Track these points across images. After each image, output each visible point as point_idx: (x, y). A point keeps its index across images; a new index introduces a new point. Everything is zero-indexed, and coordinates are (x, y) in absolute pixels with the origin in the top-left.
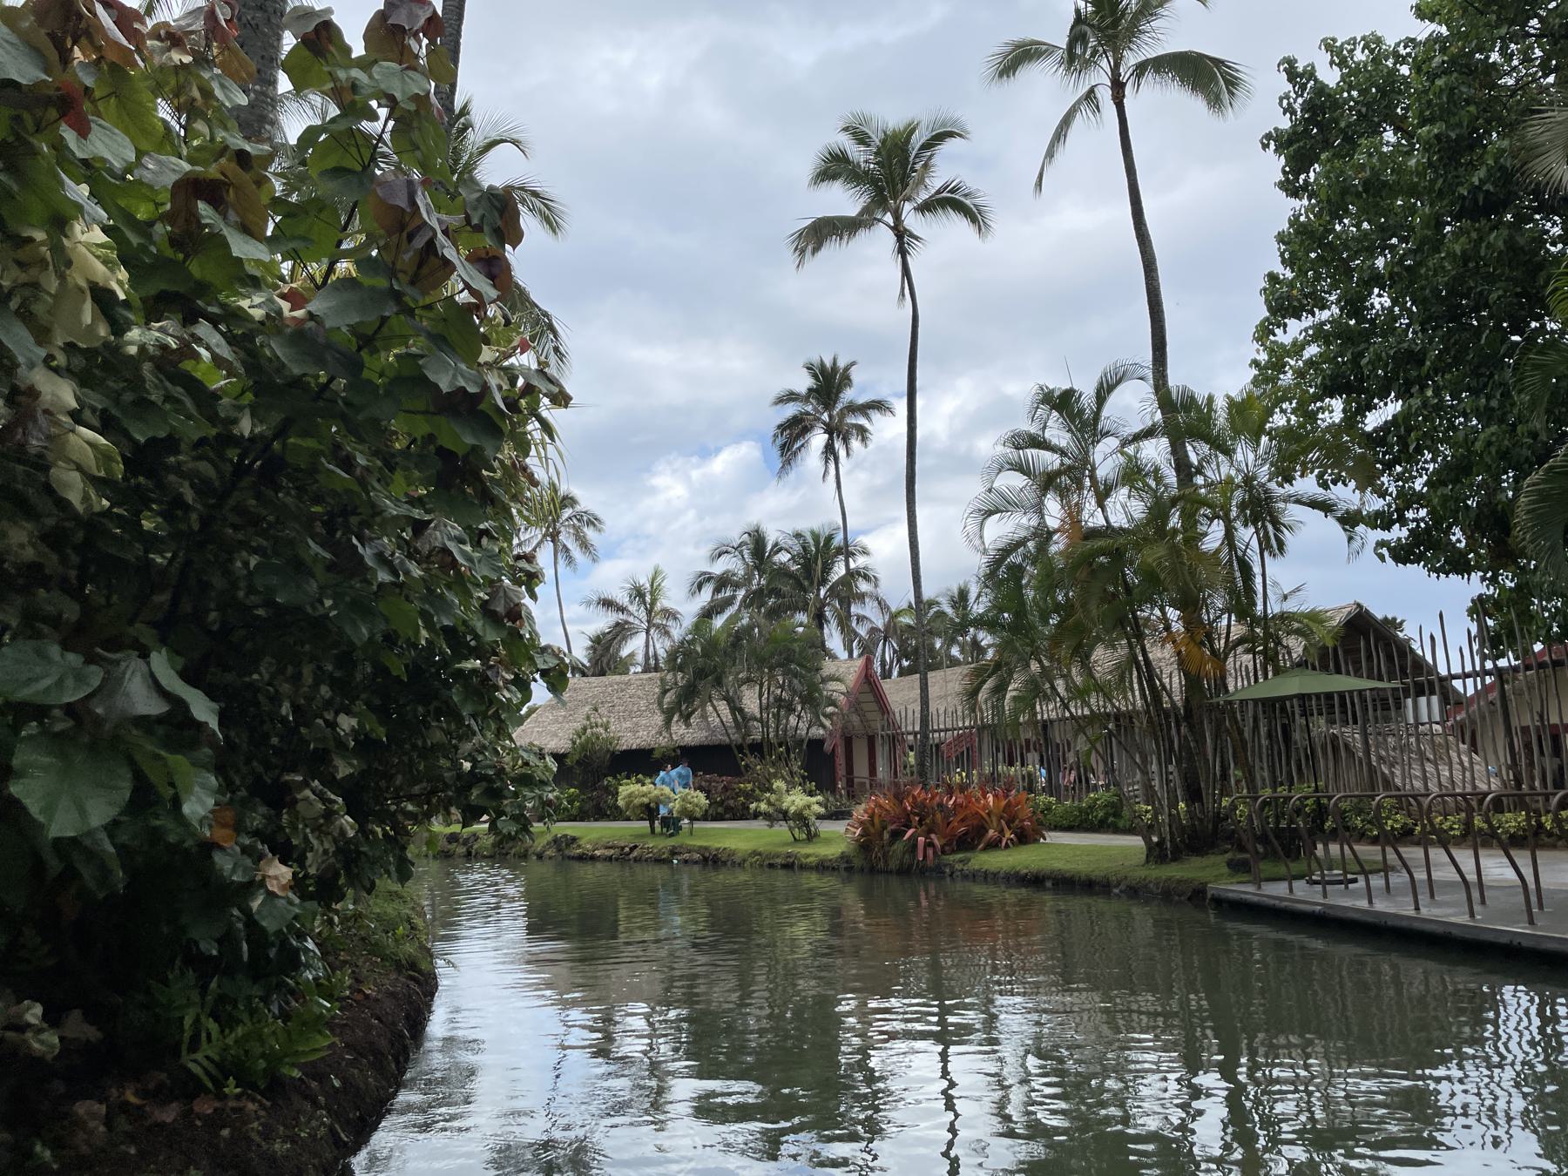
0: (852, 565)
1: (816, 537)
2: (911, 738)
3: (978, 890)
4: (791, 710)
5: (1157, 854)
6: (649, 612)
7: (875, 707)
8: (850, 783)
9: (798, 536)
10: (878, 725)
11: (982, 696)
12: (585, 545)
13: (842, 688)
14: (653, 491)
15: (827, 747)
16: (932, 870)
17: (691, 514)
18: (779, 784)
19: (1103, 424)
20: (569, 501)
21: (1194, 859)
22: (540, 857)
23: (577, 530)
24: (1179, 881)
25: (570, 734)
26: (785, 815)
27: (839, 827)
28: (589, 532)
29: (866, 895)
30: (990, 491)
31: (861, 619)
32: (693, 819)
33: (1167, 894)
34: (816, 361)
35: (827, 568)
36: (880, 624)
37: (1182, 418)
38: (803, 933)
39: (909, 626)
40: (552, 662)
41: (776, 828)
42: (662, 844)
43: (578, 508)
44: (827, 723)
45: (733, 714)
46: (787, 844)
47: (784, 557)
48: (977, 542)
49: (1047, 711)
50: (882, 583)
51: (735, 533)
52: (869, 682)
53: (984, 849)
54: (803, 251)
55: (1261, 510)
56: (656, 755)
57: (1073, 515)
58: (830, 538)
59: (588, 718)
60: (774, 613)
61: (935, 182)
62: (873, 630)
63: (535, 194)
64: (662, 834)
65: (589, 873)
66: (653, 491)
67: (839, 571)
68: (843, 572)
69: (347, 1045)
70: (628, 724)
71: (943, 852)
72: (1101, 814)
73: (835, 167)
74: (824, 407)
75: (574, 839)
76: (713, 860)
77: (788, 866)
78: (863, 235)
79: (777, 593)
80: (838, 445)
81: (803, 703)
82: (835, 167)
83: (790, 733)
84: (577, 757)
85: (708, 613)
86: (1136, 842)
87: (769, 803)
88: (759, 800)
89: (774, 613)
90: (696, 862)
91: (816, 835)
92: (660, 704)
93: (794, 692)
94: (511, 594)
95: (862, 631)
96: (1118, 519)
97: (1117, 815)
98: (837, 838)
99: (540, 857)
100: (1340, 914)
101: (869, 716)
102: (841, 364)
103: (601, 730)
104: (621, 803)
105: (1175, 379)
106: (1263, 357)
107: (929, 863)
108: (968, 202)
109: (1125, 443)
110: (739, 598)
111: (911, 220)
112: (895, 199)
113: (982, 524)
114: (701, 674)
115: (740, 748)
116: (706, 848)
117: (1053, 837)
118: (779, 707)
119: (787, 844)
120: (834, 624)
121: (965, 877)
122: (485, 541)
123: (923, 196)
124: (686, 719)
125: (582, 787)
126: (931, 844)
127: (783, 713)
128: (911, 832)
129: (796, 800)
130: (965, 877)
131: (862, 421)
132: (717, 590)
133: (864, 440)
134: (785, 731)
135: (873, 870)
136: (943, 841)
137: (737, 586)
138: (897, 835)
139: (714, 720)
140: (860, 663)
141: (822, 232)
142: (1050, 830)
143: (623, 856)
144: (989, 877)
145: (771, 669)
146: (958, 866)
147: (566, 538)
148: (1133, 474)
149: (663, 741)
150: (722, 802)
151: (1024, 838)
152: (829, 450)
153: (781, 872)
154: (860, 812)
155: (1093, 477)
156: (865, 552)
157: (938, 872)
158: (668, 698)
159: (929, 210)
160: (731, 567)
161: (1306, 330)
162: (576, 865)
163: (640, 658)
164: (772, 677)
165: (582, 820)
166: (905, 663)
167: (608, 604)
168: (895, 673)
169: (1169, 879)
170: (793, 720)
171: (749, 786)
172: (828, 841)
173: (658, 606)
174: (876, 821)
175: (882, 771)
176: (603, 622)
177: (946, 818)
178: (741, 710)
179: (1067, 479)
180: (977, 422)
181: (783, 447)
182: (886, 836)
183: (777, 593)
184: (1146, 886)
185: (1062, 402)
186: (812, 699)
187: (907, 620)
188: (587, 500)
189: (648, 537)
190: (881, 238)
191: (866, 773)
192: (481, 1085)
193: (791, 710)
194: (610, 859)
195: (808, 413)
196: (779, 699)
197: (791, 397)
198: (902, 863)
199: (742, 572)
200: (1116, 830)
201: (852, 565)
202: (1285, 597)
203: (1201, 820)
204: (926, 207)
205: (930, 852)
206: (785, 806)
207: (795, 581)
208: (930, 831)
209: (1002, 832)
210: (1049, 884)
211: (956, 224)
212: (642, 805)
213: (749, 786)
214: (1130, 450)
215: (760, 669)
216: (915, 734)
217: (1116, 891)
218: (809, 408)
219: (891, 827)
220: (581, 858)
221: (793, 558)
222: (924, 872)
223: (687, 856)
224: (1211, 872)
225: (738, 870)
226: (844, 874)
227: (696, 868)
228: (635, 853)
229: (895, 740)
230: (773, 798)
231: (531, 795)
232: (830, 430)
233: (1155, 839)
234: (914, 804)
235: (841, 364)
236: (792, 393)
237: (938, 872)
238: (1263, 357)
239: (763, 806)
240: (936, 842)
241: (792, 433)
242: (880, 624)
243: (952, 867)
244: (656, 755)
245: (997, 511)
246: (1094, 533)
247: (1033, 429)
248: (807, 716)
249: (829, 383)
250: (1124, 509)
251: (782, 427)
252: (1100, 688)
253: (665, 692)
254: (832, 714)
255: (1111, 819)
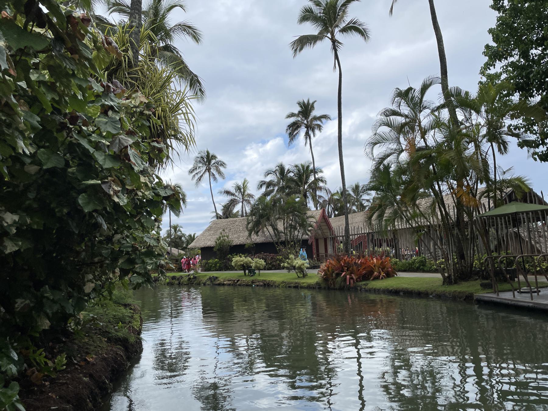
0: (317, 176)
1: (303, 166)
2: (341, 238)
3: (372, 297)
4: (295, 228)
5: (447, 281)
6: (243, 195)
7: (326, 227)
8: (318, 255)
9: (296, 166)
10: (328, 234)
11: (374, 217)
12: (220, 172)
13: (315, 220)
14: (246, 156)
15: (309, 242)
16: (352, 288)
17: (259, 164)
18: (291, 256)
19: (425, 103)
20: (214, 157)
21: (463, 283)
22: (205, 284)
23: (217, 167)
24: (459, 292)
25: (215, 239)
26: (294, 268)
27: (315, 272)
28: (221, 169)
29: (328, 300)
30: (375, 134)
31: (320, 197)
32: (259, 269)
33: (455, 298)
34: (301, 101)
35: (308, 177)
36: (327, 199)
37: (454, 99)
38: (304, 311)
39: (338, 199)
40: (169, 193)
41: (291, 272)
42: (249, 279)
43: (217, 160)
44: (309, 233)
45: (274, 231)
46: (296, 279)
47: (291, 174)
48: (371, 156)
49: (399, 225)
50: (328, 183)
51: (273, 166)
52: (325, 218)
53: (373, 280)
54: (296, 50)
55: (494, 135)
56: (246, 247)
57: (412, 143)
58: (308, 167)
59: (221, 234)
60: (288, 194)
61: (347, 19)
62: (325, 201)
63: (190, 27)
64: (249, 275)
65: (222, 290)
66: (246, 156)
67: (312, 179)
68: (313, 179)
69: (60, 397)
70: (236, 236)
71: (357, 281)
72: (417, 265)
73: (307, 16)
74: (305, 119)
75: (217, 278)
76: (267, 285)
77: (296, 287)
78: (319, 43)
79: (290, 188)
80: (311, 132)
81: (300, 226)
82: (307, 16)
83: (295, 238)
84: (217, 248)
85: (266, 194)
86: (439, 276)
87: (288, 263)
88: (284, 262)
89: (288, 194)
90: (261, 286)
91: (306, 275)
92: (247, 228)
93: (296, 222)
94: (123, 142)
95: (321, 201)
96: (431, 142)
97: (424, 265)
98: (315, 276)
99: (205, 284)
100: (542, 307)
101: (325, 231)
102: (311, 102)
103: (226, 238)
104: (233, 264)
105: (452, 84)
106: (484, 79)
107: (352, 285)
108: (360, 28)
109: (433, 111)
110: (276, 190)
111: (338, 36)
112: (331, 27)
113: (373, 148)
114: (261, 216)
115: (277, 243)
116: (265, 281)
117: (401, 275)
118: (291, 228)
119: (296, 279)
120: (310, 198)
121: (366, 291)
122: (110, 113)
123: (342, 25)
124: (257, 233)
125: (220, 259)
126: (352, 278)
127: (292, 230)
128: (344, 274)
129: (298, 262)
130: (366, 291)
131: (319, 122)
132: (268, 187)
133: (320, 130)
134: (293, 237)
135: (329, 289)
136: (357, 277)
137: (274, 185)
138: (338, 275)
139: (267, 233)
140: (321, 211)
141: (303, 42)
142: (397, 272)
143: (234, 284)
144: (377, 291)
145: (287, 214)
146: (364, 287)
147: (213, 170)
148: (437, 124)
149: (249, 241)
150: (271, 263)
151: (389, 275)
152: (307, 135)
153: (293, 290)
154: (323, 266)
155: (420, 125)
156: (321, 172)
157: (355, 289)
158: (250, 225)
159: (345, 31)
160: (272, 179)
161: (503, 67)
162: (217, 287)
163: (240, 213)
164: (288, 217)
165: (220, 270)
166: (337, 213)
167: (228, 193)
168: (333, 216)
169: (455, 291)
170: (296, 233)
171: (281, 257)
172: (311, 277)
173: (246, 193)
174: (330, 269)
175: (330, 251)
176: (226, 199)
177: (358, 267)
178: (277, 230)
179: (410, 126)
180: (360, 128)
181: (290, 134)
182: (334, 275)
183: (290, 188)
184: (444, 294)
185: (404, 95)
186: (303, 225)
187: (336, 197)
188: (219, 158)
189: (244, 172)
190: (327, 43)
191: (324, 252)
192: (191, 362)
193: (295, 228)
194: (229, 285)
195: (299, 121)
196: (291, 225)
197: (292, 115)
198: (340, 286)
199: (276, 180)
200: (424, 271)
201: (317, 176)
202: (504, 173)
203: (465, 267)
204: (344, 30)
205: (352, 281)
206: (294, 264)
207: (297, 182)
208: (351, 273)
209: (380, 273)
210: (401, 294)
211: (355, 37)
212: (241, 265)
213: (281, 257)
214: (436, 113)
215: (284, 214)
216: (343, 237)
217: (431, 296)
218: (299, 119)
219: (336, 272)
220: (219, 285)
221: (295, 175)
222: (349, 289)
223: (258, 283)
224: (472, 287)
225: (277, 289)
226: (318, 290)
227: (261, 288)
228: (239, 283)
229: (334, 239)
230: (290, 261)
231: (150, 262)
232: (307, 127)
233: (446, 275)
234: (345, 263)
235: (311, 102)
236: (293, 114)
237: (355, 289)
238: (484, 79)
239: (286, 265)
240: (354, 277)
241: (294, 128)
242: (327, 199)
243: (361, 287)
244: (246, 247)
245: (380, 143)
246: (420, 149)
247: (394, 107)
248: (301, 231)
249: (306, 109)
250: (434, 138)
251: (290, 126)
252: (422, 215)
253: (249, 223)
254: (311, 230)
255: (421, 267)
